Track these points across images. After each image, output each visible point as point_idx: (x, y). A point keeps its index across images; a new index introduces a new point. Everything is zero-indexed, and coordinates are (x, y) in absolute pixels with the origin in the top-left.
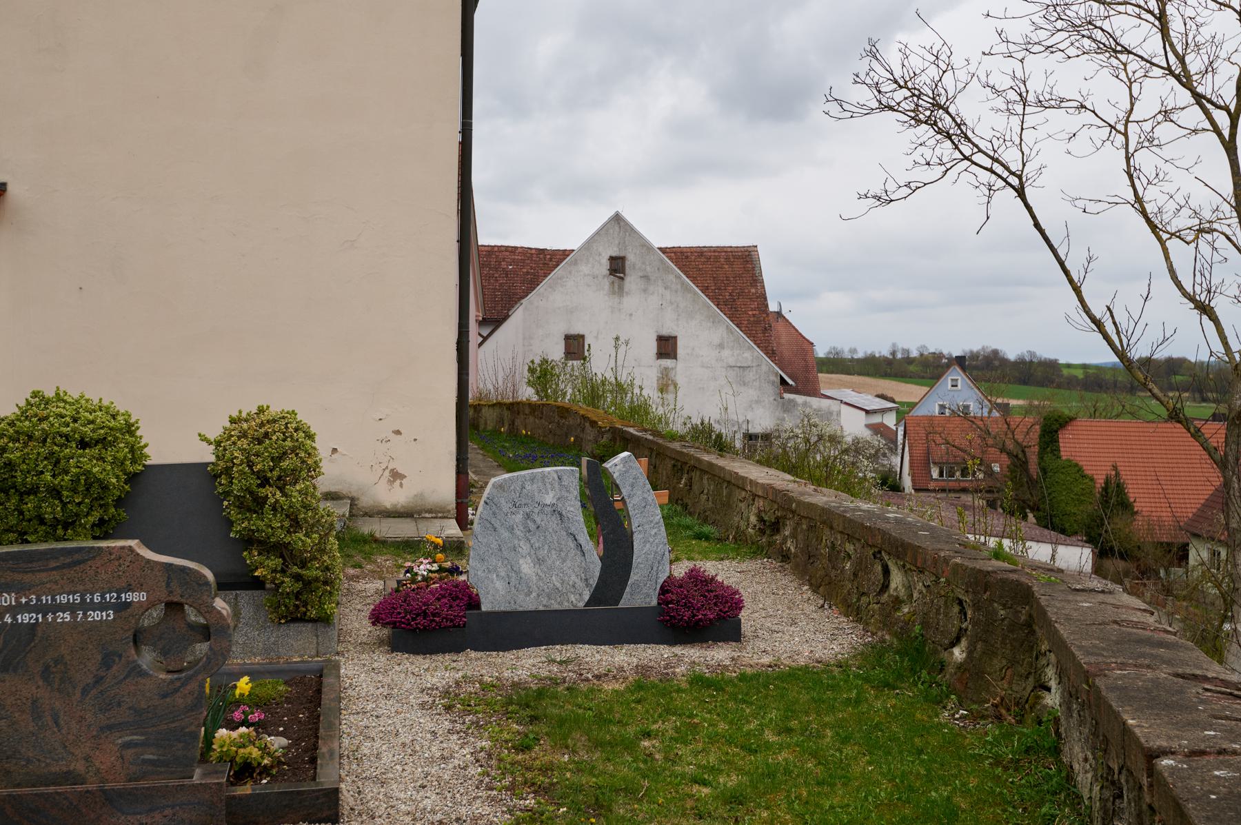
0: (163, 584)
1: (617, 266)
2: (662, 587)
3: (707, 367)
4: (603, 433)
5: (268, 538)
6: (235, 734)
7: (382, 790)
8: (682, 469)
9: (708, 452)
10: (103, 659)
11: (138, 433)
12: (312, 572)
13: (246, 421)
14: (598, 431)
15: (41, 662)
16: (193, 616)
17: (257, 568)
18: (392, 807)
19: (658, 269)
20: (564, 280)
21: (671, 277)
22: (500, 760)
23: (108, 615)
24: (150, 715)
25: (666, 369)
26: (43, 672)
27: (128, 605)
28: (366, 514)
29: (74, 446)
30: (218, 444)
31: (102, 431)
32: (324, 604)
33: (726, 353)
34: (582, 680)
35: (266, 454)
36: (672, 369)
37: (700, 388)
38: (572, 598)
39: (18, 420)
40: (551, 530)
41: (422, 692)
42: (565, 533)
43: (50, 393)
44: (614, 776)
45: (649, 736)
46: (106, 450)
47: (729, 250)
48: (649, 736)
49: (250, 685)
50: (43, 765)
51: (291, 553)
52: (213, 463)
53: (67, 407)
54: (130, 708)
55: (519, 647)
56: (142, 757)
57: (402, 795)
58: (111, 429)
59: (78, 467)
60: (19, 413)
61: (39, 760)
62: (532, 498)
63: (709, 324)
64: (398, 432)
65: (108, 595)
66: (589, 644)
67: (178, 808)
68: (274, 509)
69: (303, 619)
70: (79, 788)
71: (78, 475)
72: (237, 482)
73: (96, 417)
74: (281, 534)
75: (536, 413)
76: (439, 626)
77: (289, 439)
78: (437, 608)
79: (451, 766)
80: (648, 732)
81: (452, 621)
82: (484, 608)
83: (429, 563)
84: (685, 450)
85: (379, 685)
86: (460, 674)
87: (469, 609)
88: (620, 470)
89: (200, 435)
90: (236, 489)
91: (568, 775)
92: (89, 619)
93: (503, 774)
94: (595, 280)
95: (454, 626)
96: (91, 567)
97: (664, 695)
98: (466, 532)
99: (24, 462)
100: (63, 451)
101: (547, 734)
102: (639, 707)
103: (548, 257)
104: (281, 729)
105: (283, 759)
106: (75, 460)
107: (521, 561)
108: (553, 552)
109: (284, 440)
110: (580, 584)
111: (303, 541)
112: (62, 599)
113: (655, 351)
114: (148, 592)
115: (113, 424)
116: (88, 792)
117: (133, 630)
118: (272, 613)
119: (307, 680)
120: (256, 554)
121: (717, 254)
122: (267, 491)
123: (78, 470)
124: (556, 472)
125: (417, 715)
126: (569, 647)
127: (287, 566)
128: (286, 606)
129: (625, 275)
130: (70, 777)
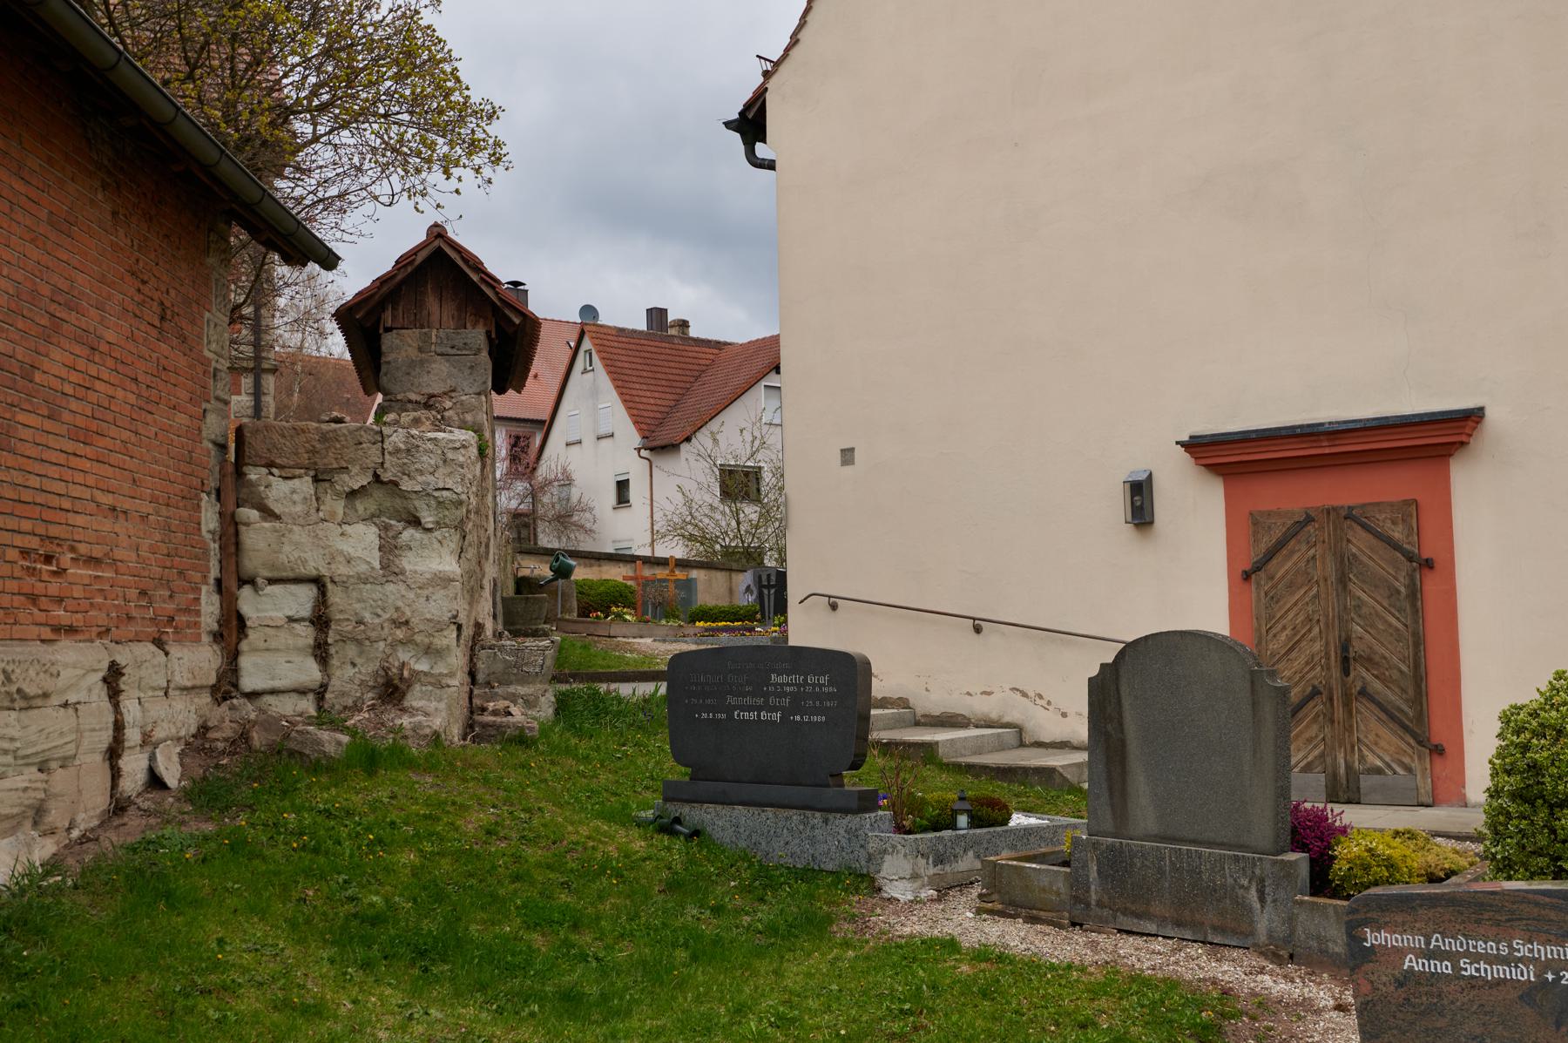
39: (1541, 709)
60: (1542, 700)
99: (1553, 764)
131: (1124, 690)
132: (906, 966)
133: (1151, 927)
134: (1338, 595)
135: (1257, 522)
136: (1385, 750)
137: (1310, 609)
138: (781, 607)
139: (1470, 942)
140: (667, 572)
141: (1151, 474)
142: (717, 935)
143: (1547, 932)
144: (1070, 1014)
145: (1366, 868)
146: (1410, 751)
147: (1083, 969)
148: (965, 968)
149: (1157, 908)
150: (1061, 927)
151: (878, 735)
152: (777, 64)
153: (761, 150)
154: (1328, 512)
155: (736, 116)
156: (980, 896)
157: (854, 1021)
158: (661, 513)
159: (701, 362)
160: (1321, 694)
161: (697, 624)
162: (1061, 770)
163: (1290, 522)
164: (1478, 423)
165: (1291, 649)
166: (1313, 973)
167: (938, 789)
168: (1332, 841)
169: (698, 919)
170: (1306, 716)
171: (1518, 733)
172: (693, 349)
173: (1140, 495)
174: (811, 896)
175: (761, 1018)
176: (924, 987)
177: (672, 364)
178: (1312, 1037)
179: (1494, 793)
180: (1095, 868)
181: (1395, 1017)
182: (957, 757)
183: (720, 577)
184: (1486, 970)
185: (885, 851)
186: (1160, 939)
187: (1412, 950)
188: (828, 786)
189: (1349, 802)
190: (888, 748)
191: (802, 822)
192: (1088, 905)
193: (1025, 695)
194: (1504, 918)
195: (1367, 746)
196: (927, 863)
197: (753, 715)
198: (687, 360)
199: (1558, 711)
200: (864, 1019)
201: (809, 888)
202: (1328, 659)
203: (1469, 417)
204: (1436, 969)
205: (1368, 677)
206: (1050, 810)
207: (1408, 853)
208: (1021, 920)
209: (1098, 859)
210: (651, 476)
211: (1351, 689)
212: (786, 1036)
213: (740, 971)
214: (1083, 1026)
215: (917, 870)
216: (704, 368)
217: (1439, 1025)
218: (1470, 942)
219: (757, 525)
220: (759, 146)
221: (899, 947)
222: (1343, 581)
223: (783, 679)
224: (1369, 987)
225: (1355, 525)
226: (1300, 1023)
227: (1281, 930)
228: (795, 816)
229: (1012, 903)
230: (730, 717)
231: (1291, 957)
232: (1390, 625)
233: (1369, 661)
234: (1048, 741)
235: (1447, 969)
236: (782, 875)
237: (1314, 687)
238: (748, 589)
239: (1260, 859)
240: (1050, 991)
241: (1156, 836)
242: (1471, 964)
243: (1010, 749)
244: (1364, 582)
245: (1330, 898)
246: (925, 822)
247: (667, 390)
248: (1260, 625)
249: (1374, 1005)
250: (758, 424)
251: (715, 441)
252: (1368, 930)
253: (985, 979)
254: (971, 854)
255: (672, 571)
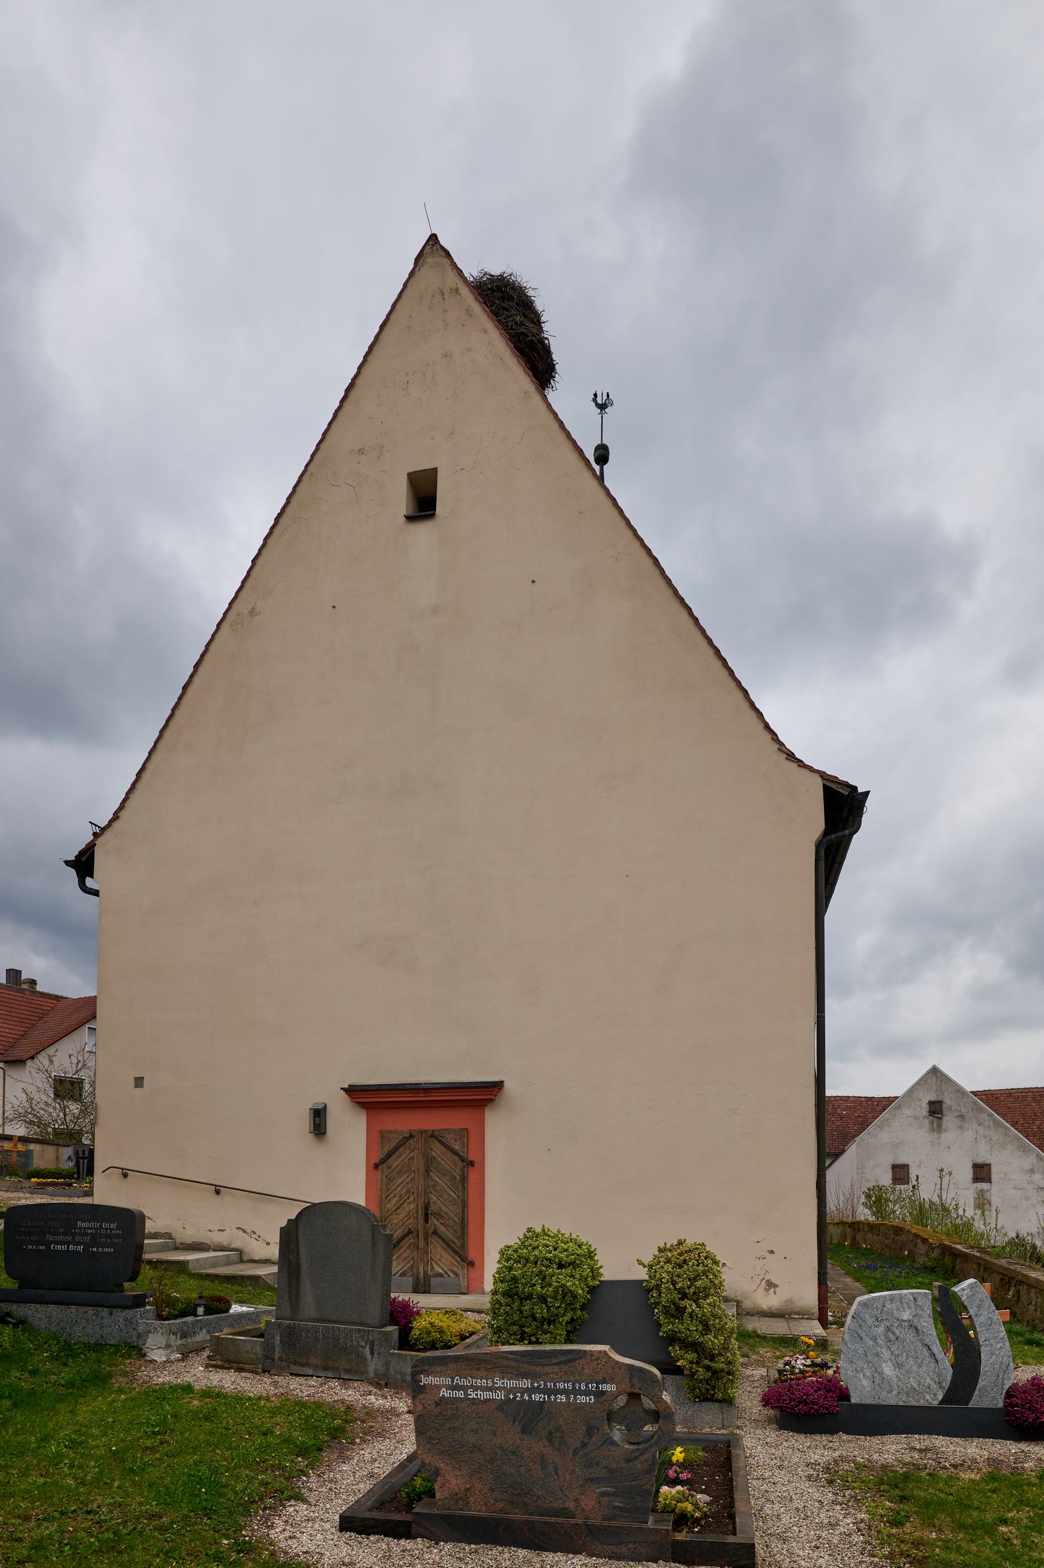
0: (628, 1379)
1: (936, 1109)
2: (1008, 1392)
3: (1019, 1189)
4: (933, 1249)
5: (687, 1338)
6: (674, 1491)
7: (785, 1546)
8: (1009, 1283)
9: (1034, 1269)
10: (587, 1430)
11: (596, 1258)
12: (720, 1365)
13: (670, 1251)
14: (929, 1247)
15: (547, 1429)
16: (648, 1403)
17: (678, 1360)
18: (795, 1562)
19: (972, 1109)
20: (890, 1121)
21: (984, 1116)
22: (879, 1532)
23: (590, 1400)
24: (618, 1474)
25: (981, 1191)
26: (548, 1436)
27: (603, 1393)
28: (748, 1314)
29: (555, 1267)
30: (651, 1267)
31: (573, 1257)
32: (728, 1389)
33: (1037, 1177)
34: (941, 1468)
35: (685, 1276)
36: (988, 1190)
37: (1013, 1207)
38: (928, 1397)
39: (519, 1248)
40: (908, 1341)
41: (808, 1466)
42: (920, 1344)
43: (538, 1230)
44: (979, 1556)
45: (1006, 1522)
46: (575, 1270)
47: (1036, 1090)
48: (1006, 1522)
49: (683, 1454)
50: (548, 1502)
51: (703, 1349)
52: (647, 1281)
53: (550, 1239)
54: (605, 1468)
55: (883, 1434)
56: (613, 1504)
57: (801, 1553)
58: (578, 1255)
59: (558, 1282)
60: (520, 1243)
61: (545, 1498)
62: (892, 1314)
63: (1020, 1153)
64: (772, 1252)
65: (590, 1385)
66: (943, 1436)
67: (638, 1544)
68: (691, 1316)
69: (712, 1399)
70: (572, 1521)
71: (557, 1287)
72: (664, 1296)
73: (569, 1247)
74: (696, 1336)
75: (874, 1231)
76: (817, 1413)
77: (701, 1265)
78: (815, 1398)
79: (837, 1532)
80: (1005, 1519)
81: (827, 1409)
82: (853, 1401)
83: (804, 1359)
84: (1012, 1267)
85: (773, 1457)
86: (837, 1454)
87: (841, 1401)
88: (967, 1294)
89: (638, 1260)
90: (663, 1300)
91: (937, 1551)
92: (578, 1401)
93: (881, 1544)
94: (917, 1120)
95: (829, 1413)
96: (579, 1364)
97: (1016, 1488)
98: (827, 1331)
99: (523, 1277)
100: (548, 1270)
101: (915, 1513)
102: (995, 1496)
103: (876, 1103)
104: (703, 1487)
105: (708, 1513)
106: (556, 1277)
107: (883, 1365)
108: (911, 1359)
109: (698, 1266)
110: (934, 1386)
111: (712, 1342)
112: (561, 1385)
113: (972, 1176)
114: (617, 1384)
115: (579, 1252)
116: (577, 1524)
117: (607, 1411)
118: (689, 1393)
119: (718, 1448)
120: (678, 1349)
121: (1024, 1094)
122: (686, 1303)
123: (557, 1284)
124: (912, 1294)
125: (804, 1485)
126: (926, 1437)
127: (700, 1359)
128: (699, 1389)
129: (942, 1115)
130: (564, 1512)
131: (300, 1234)
132: (158, 1403)
133: (310, 1372)
134: (424, 1179)
135: (383, 1136)
136: (444, 1264)
137: (409, 1186)
138: (90, 1172)
139: (474, 1380)
140: (12, 1145)
141: (326, 1105)
142: (32, 1389)
143: (511, 1373)
144: (258, 1428)
145: (429, 1333)
146: (457, 1264)
147: (268, 1399)
148: (196, 1402)
149: (313, 1360)
150: (257, 1373)
151: (146, 1256)
152: (103, 830)
153: (89, 882)
154: (422, 1133)
155: (73, 858)
156: (209, 1357)
157: (122, 1441)
158: (10, 1105)
159: (44, 1008)
160: (413, 1233)
161: (32, 1180)
162: (264, 1277)
163: (401, 1137)
164: (500, 1089)
165: (398, 1208)
166: (397, 1393)
167: (183, 1291)
168: (412, 1319)
169: (20, 1379)
170: (404, 1246)
171: (507, 1261)
172: (39, 999)
173: (319, 1120)
174: (99, 1361)
175: (59, 1443)
176: (169, 1416)
177: (23, 1008)
178: (394, 1430)
179: (495, 1292)
180: (279, 1338)
181: (434, 1422)
182: (200, 1269)
183: (50, 1150)
184: (480, 1394)
185: (149, 1332)
186: (314, 1378)
187: (444, 1386)
188: (114, 1292)
189: (424, 1292)
190: (155, 1264)
191: (94, 1314)
192: (273, 1360)
193: (245, 1231)
194: (490, 1367)
195: (436, 1262)
196: (176, 1338)
197: (64, 1247)
198: (35, 1006)
199: (527, 1249)
200: (128, 1439)
201: (98, 1356)
202: (417, 1214)
203: (496, 1086)
204: (456, 1395)
205: (438, 1224)
206: (256, 1301)
207: (451, 1323)
208: (233, 1371)
209: (281, 1333)
210: (4, 1079)
211: (428, 1230)
212: (76, 1454)
213: (47, 1412)
214: (265, 1434)
215: (169, 1343)
216: (46, 1012)
217: (456, 1426)
218: (474, 1380)
219: (78, 1117)
220: (88, 880)
221: (155, 1391)
222: (427, 1171)
223: (86, 1225)
224: (422, 1407)
225: (435, 1140)
226: (388, 1423)
227: (382, 1369)
228: (91, 1311)
229: (228, 1361)
230: (48, 1248)
231: (386, 1384)
232: (451, 1196)
233: (438, 1215)
234: (257, 1259)
235: (461, 1395)
236: (79, 1348)
237: (409, 1229)
238: (69, 1158)
239: (372, 1330)
240: (247, 1413)
241: (315, 1319)
242: (473, 1392)
243: (234, 1264)
244: (438, 1172)
245: (408, 1351)
246: (176, 1312)
247: (18, 1024)
248: (382, 1194)
249: (424, 1416)
250: (82, 1053)
251: (51, 1061)
252: (423, 1376)
253: (208, 1409)
254: (204, 1331)
255: (16, 1145)
